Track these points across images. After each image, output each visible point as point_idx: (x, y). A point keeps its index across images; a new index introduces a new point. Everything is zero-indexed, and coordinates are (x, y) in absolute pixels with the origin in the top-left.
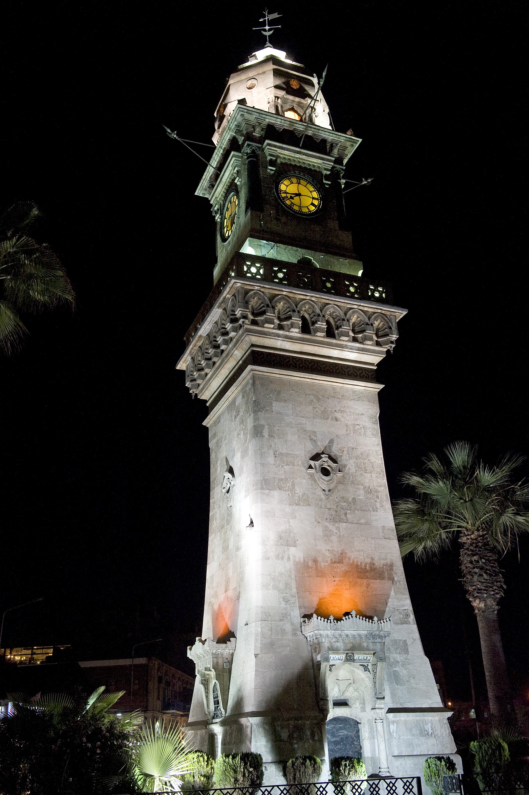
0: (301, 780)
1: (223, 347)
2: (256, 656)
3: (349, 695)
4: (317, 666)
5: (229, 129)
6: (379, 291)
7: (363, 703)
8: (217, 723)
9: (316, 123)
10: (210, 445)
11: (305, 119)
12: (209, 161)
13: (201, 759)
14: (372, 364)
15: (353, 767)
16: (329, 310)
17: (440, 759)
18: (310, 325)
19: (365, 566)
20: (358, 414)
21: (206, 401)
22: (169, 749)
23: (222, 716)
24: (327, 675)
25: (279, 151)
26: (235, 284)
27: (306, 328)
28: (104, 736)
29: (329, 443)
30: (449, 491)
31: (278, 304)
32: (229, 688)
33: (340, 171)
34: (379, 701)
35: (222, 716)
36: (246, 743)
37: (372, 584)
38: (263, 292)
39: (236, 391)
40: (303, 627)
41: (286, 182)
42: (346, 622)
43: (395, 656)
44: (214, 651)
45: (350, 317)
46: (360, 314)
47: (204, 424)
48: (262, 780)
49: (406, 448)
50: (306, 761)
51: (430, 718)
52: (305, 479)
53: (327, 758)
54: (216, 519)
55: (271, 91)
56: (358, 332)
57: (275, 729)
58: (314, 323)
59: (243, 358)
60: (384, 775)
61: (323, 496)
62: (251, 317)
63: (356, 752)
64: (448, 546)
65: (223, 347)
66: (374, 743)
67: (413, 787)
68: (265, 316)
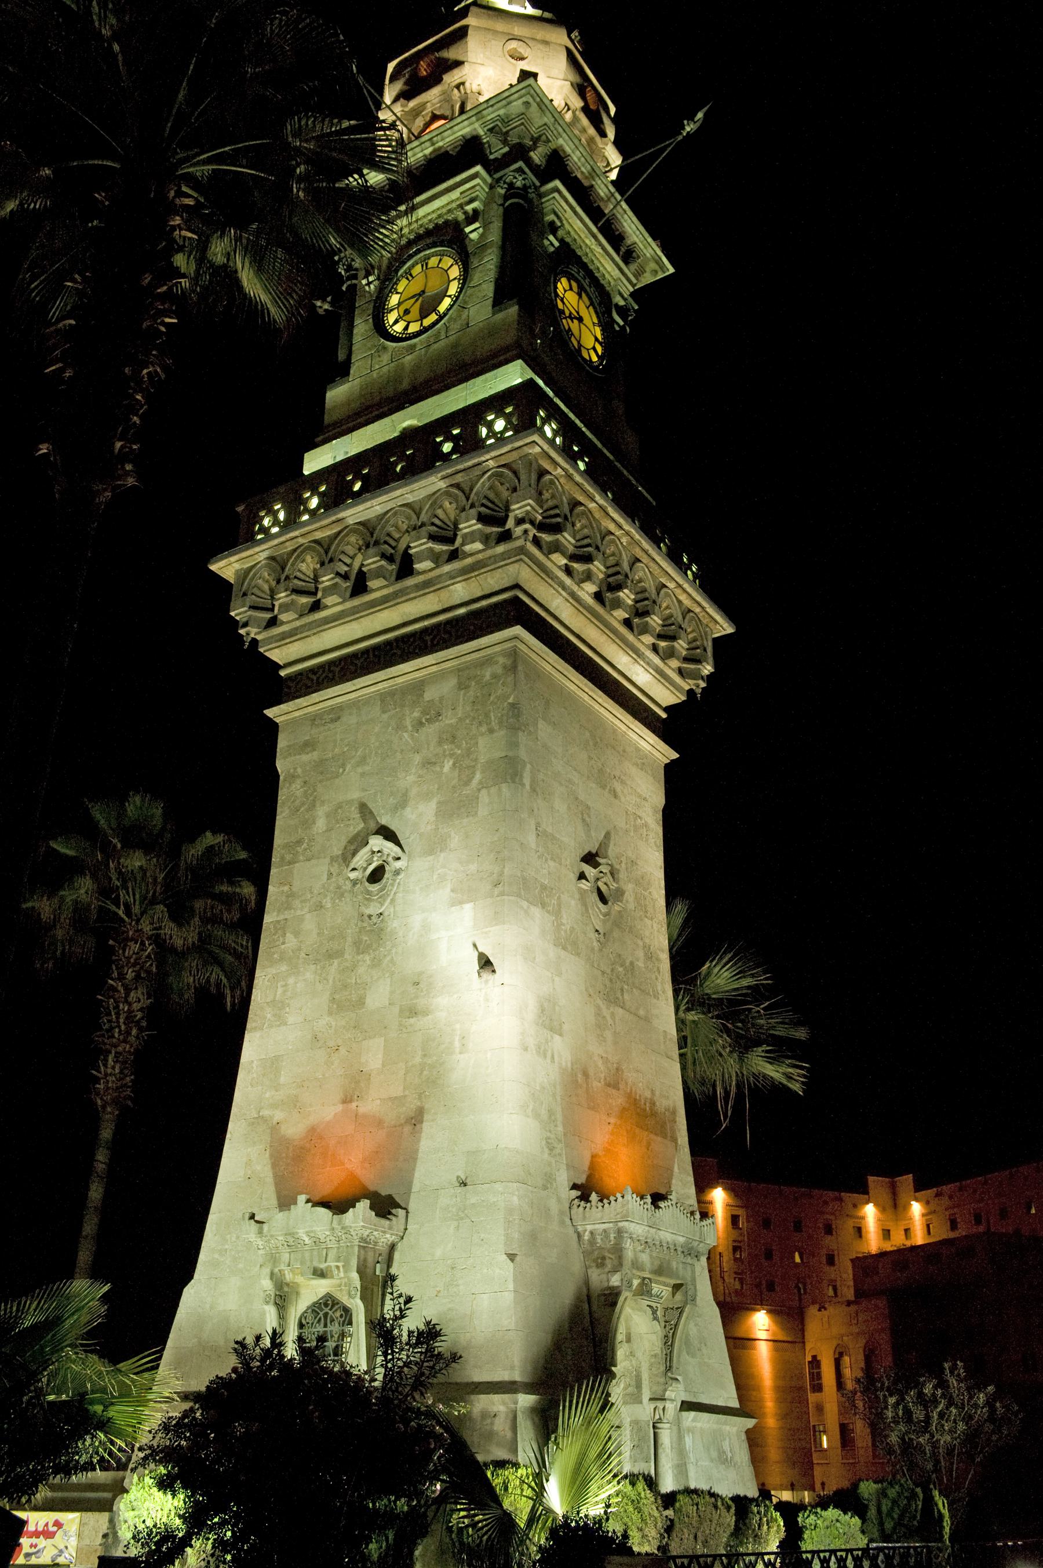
29: (605, 837)
55: (562, 87)
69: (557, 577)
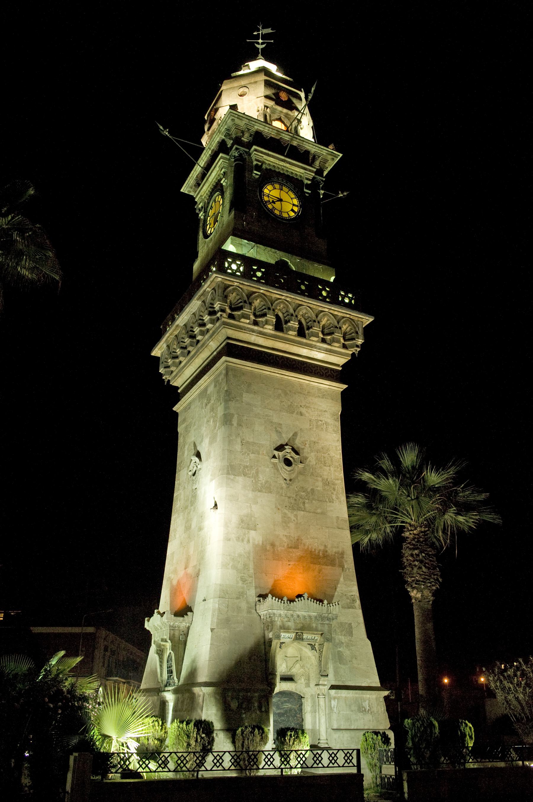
0: (249, 748)
1: (199, 338)
2: (212, 630)
3: (296, 671)
4: (268, 643)
5: (219, 132)
6: (349, 297)
7: (308, 679)
8: (169, 691)
9: (301, 135)
10: (179, 430)
11: (291, 129)
12: (197, 160)
13: (156, 723)
14: (338, 365)
15: (298, 737)
16: (302, 311)
17: (376, 733)
18: (283, 323)
19: (319, 553)
20: (321, 411)
21: (178, 388)
22: (128, 712)
23: (174, 685)
24: (277, 651)
25: (265, 157)
26: (215, 278)
27: (279, 326)
28: (66, 698)
29: (293, 435)
30: (397, 488)
31: (255, 301)
32: (183, 659)
33: (320, 182)
34: (322, 678)
35: (174, 685)
36: (197, 711)
37: (323, 570)
38: (241, 288)
39: (209, 380)
40: (257, 606)
41: (270, 187)
42: (299, 604)
43: (340, 637)
44: (172, 624)
45: (321, 319)
46: (330, 317)
47: (174, 409)
48: (213, 745)
49: (362, 447)
50: (254, 731)
51: (368, 696)
52: (268, 467)
53: (271, 728)
54: (180, 500)
55: (261, 100)
56: (327, 333)
57: (226, 699)
58: (287, 322)
59: (218, 350)
60: (322, 746)
61: (284, 486)
62: (228, 311)
63: (298, 724)
64: (391, 539)
65: (199, 338)
66: (315, 716)
67: (353, 758)
68: (242, 311)
69: (248, 328)
